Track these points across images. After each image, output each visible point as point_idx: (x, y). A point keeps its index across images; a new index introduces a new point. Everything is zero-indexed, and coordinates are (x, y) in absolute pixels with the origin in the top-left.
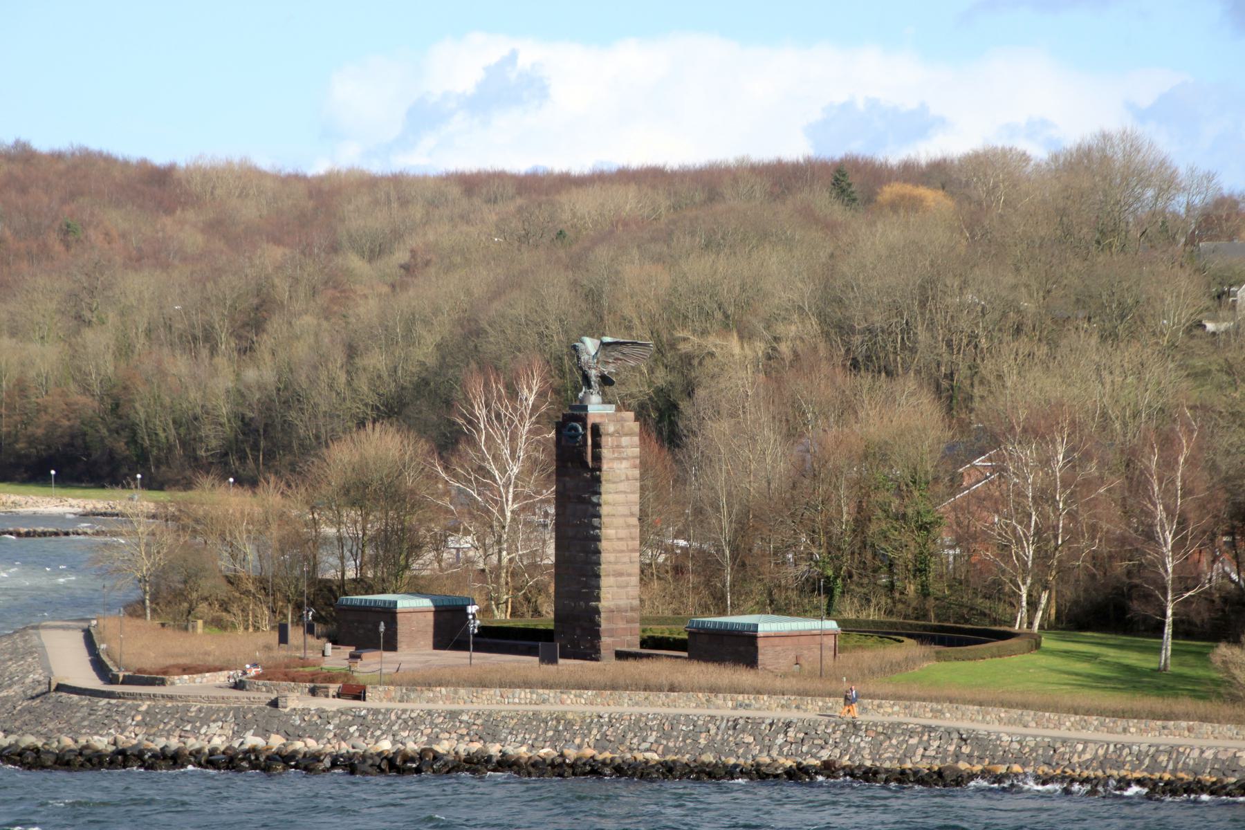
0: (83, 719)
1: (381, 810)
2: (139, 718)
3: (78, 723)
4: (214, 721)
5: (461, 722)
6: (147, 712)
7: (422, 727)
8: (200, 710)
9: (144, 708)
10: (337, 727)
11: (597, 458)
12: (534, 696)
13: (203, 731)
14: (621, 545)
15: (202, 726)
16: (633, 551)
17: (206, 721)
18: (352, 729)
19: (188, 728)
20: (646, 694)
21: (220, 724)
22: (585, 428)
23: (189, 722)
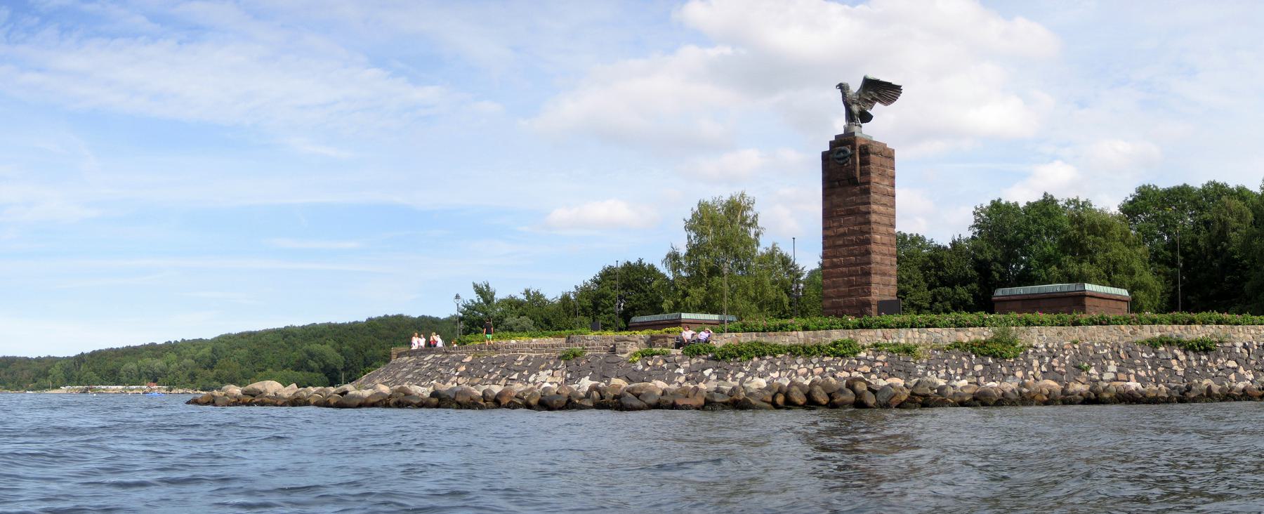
0: (408, 373)
1: (198, 472)
2: (463, 368)
3: (402, 377)
4: (544, 370)
5: (859, 360)
6: (471, 364)
7: (795, 367)
8: (528, 359)
9: (469, 359)
10: (688, 371)
11: (866, 173)
12: (924, 335)
13: (531, 379)
14: (884, 249)
15: (530, 375)
16: (892, 255)
17: (535, 370)
18: (707, 373)
19: (515, 376)
20: (1060, 328)
21: (550, 371)
22: (853, 148)
23: (516, 371)
